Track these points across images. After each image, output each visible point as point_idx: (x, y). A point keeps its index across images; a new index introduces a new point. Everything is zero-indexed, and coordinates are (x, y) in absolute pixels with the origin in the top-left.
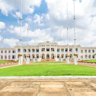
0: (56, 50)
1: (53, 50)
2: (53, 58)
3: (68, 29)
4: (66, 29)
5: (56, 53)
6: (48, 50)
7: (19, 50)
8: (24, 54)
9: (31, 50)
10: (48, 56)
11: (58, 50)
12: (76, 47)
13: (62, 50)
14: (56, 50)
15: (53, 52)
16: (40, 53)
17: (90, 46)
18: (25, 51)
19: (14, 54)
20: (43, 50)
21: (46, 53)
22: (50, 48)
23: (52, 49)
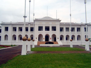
0: (58, 29)
1: (54, 29)
2: (55, 40)
3: (85, 3)
4: (84, 2)
5: (58, 33)
6: (47, 29)
7: (7, 29)
8: (46, 34)
9: (17, 29)
10: (47, 37)
11: (61, 30)
12: (26, 25)
13: (67, 29)
14: (58, 29)
15: (54, 32)
16: (36, 33)
17: (22, 20)
18: (15, 29)
19: (6, 33)
20: (40, 28)
21: (44, 33)
22: (50, 25)
23: (19, 28)
